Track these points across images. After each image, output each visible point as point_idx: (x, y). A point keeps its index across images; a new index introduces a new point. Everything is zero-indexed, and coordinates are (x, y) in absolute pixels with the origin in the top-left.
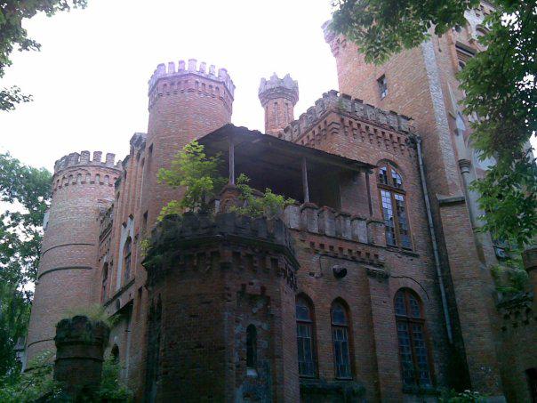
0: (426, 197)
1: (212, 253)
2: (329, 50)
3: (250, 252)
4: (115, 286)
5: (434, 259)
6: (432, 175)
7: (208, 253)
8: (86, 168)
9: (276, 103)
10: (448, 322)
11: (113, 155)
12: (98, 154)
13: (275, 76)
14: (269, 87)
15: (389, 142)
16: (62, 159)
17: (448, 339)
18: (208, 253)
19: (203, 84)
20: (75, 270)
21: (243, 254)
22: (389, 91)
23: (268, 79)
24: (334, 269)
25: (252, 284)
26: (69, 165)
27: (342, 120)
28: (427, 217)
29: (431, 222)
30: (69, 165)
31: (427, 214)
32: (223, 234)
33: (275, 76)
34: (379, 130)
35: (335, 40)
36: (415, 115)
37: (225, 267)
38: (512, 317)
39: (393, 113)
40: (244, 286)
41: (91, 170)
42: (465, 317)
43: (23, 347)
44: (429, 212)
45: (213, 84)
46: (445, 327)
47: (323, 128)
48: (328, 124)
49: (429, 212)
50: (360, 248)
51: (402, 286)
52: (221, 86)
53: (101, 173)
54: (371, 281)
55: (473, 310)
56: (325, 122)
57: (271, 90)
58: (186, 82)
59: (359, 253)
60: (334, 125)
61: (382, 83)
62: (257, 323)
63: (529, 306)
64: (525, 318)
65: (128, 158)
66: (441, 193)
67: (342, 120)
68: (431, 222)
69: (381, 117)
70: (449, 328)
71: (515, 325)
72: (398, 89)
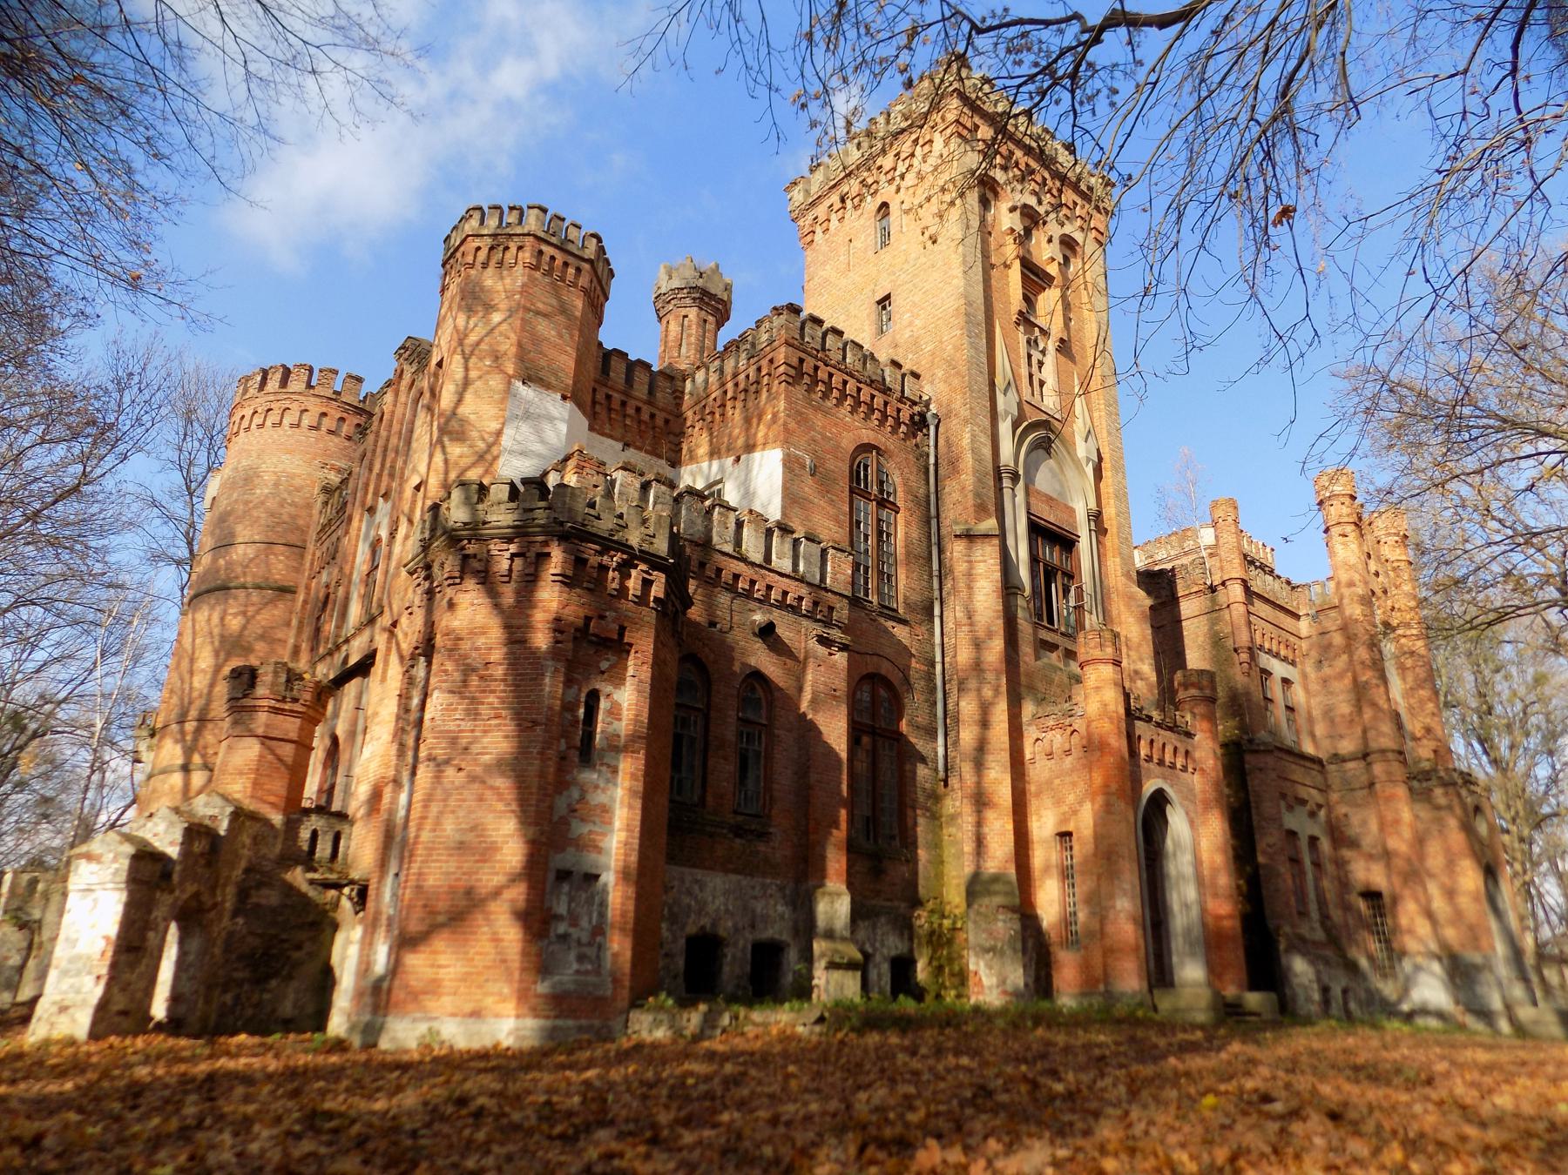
27: (801, 361)
31: (930, 553)
45: (571, 260)
51: (871, 670)
63: (1076, 726)
65: (389, 384)
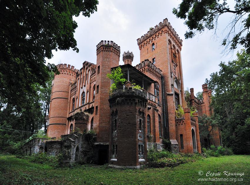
0: (163, 92)
1: (133, 99)
2: (139, 47)
3: (141, 100)
4: (78, 105)
5: (163, 107)
6: (165, 87)
7: (132, 99)
8: (66, 69)
9: (128, 60)
10: (165, 122)
11: (74, 67)
12: (69, 65)
13: (128, 52)
14: (127, 55)
15: (157, 77)
16: (58, 65)
17: (165, 126)
18: (132, 99)
19: (114, 50)
20: (64, 99)
21: (140, 101)
22: (156, 62)
23: (126, 52)
24: (148, 107)
25: (141, 109)
26: (61, 67)
27: (149, 68)
28: (163, 97)
29: (164, 98)
30: (61, 67)
32: (136, 95)
33: (128, 52)
34: (156, 73)
35: (141, 45)
36: (163, 70)
37: (136, 103)
38: (179, 123)
39: (159, 69)
40: (139, 109)
41: (67, 70)
42: (170, 122)
43: (48, 118)
44: (164, 96)
45: (117, 51)
46: (164, 123)
47: (144, 70)
48: (146, 69)
49: (164, 96)
50: (153, 103)
52: (118, 52)
53: (70, 72)
54: (155, 111)
55: (172, 120)
56: (145, 68)
57: (127, 56)
58: (110, 48)
59: (153, 104)
60: (147, 69)
61: (154, 60)
62: (141, 119)
64: (182, 123)
66: (167, 92)
67: (149, 68)
68: (164, 98)
69: (157, 69)
70: (165, 124)
71: (179, 125)
72: (158, 63)
